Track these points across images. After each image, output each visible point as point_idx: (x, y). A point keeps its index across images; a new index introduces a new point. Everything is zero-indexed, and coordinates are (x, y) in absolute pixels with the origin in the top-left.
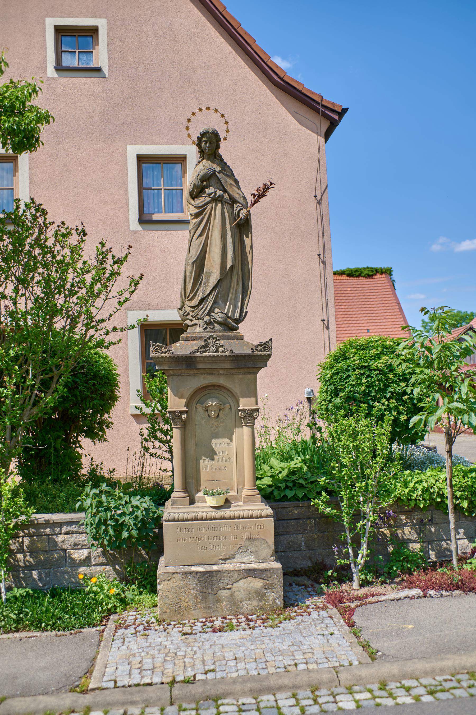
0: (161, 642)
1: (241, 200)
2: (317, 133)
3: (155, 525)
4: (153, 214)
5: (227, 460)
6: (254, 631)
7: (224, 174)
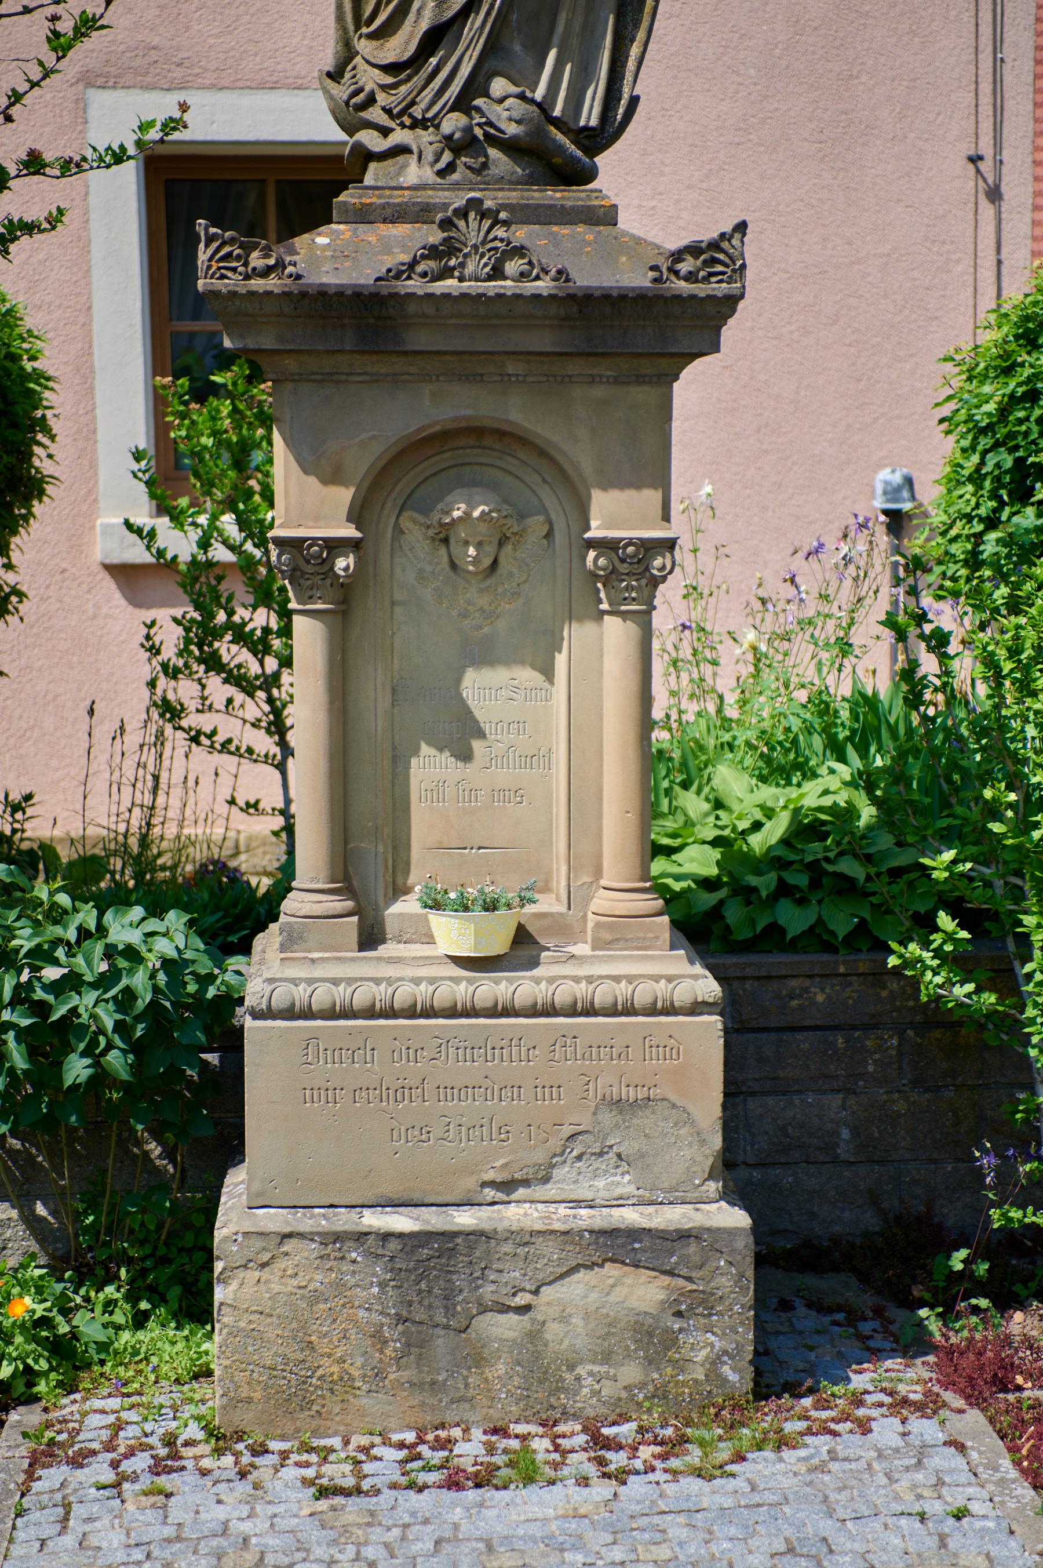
3: (207, 1030)
6: (622, 1490)
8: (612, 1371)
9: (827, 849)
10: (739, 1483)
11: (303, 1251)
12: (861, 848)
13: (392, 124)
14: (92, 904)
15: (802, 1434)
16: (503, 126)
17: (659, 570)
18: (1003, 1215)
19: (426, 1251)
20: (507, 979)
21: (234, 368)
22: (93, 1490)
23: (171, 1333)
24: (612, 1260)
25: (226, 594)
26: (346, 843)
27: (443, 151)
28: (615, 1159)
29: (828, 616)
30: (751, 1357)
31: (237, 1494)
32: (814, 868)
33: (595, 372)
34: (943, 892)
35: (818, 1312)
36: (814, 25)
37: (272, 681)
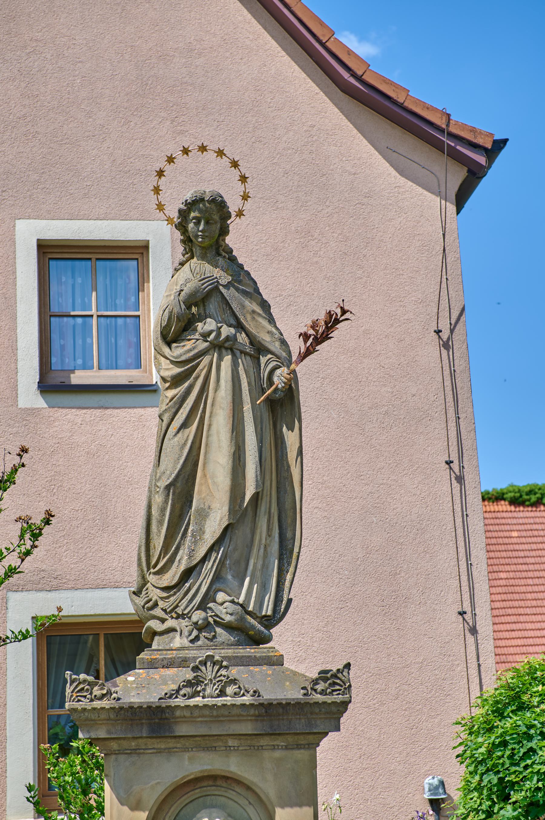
1: (276, 347)
2: (439, 194)
4: (73, 371)
7: (237, 289)
13: (166, 617)
27: (193, 629)
33: (275, 743)
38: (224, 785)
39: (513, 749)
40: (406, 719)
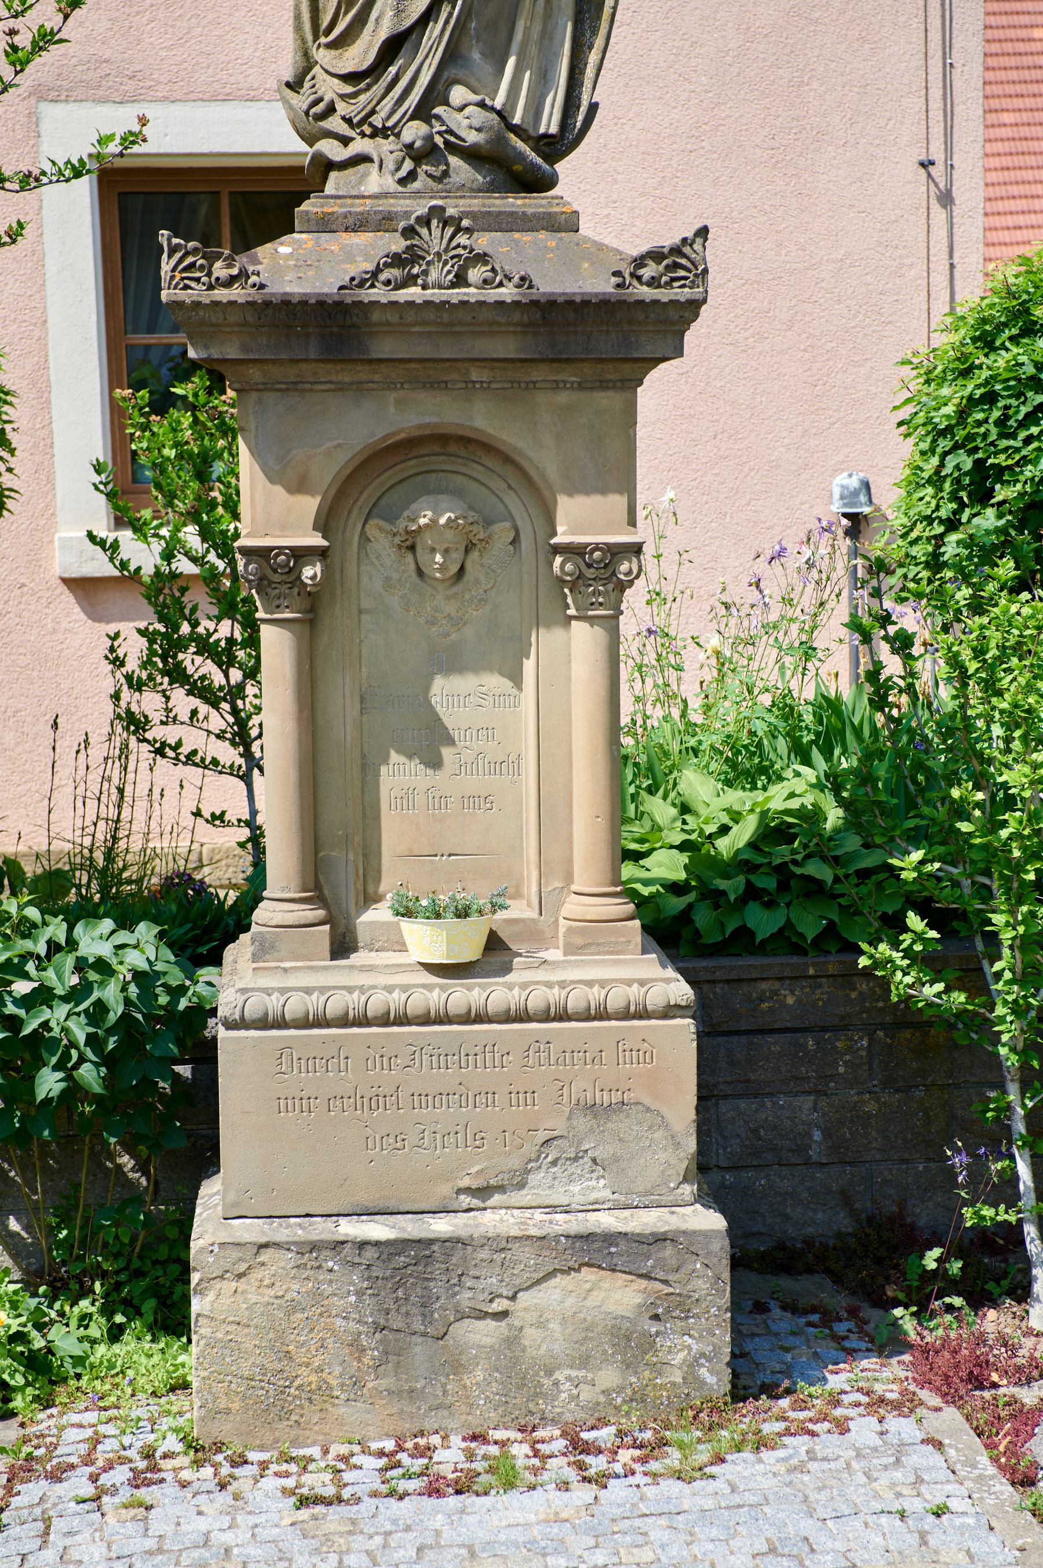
0: (207, 1535)
3: (179, 1042)
5: (498, 766)
8: (590, 1376)
9: (794, 852)
10: (720, 1485)
11: (279, 1261)
12: (829, 850)
13: (351, 133)
14: (61, 917)
15: (780, 1435)
16: (463, 134)
17: (626, 574)
18: (975, 1213)
19: (402, 1259)
20: (480, 985)
21: (196, 380)
22: (73, 1504)
23: (147, 1346)
24: (588, 1265)
25: (189, 606)
26: (316, 851)
28: (590, 1163)
29: (791, 620)
30: (728, 1359)
31: (217, 1505)
32: (782, 870)
33: (559, 377)
34: (911, 892)
35: (793, 1313)
36: (765, 32)
37: (237, 692)
38: (462, 452)
39: (1007, 408)
40: (805, 368)
